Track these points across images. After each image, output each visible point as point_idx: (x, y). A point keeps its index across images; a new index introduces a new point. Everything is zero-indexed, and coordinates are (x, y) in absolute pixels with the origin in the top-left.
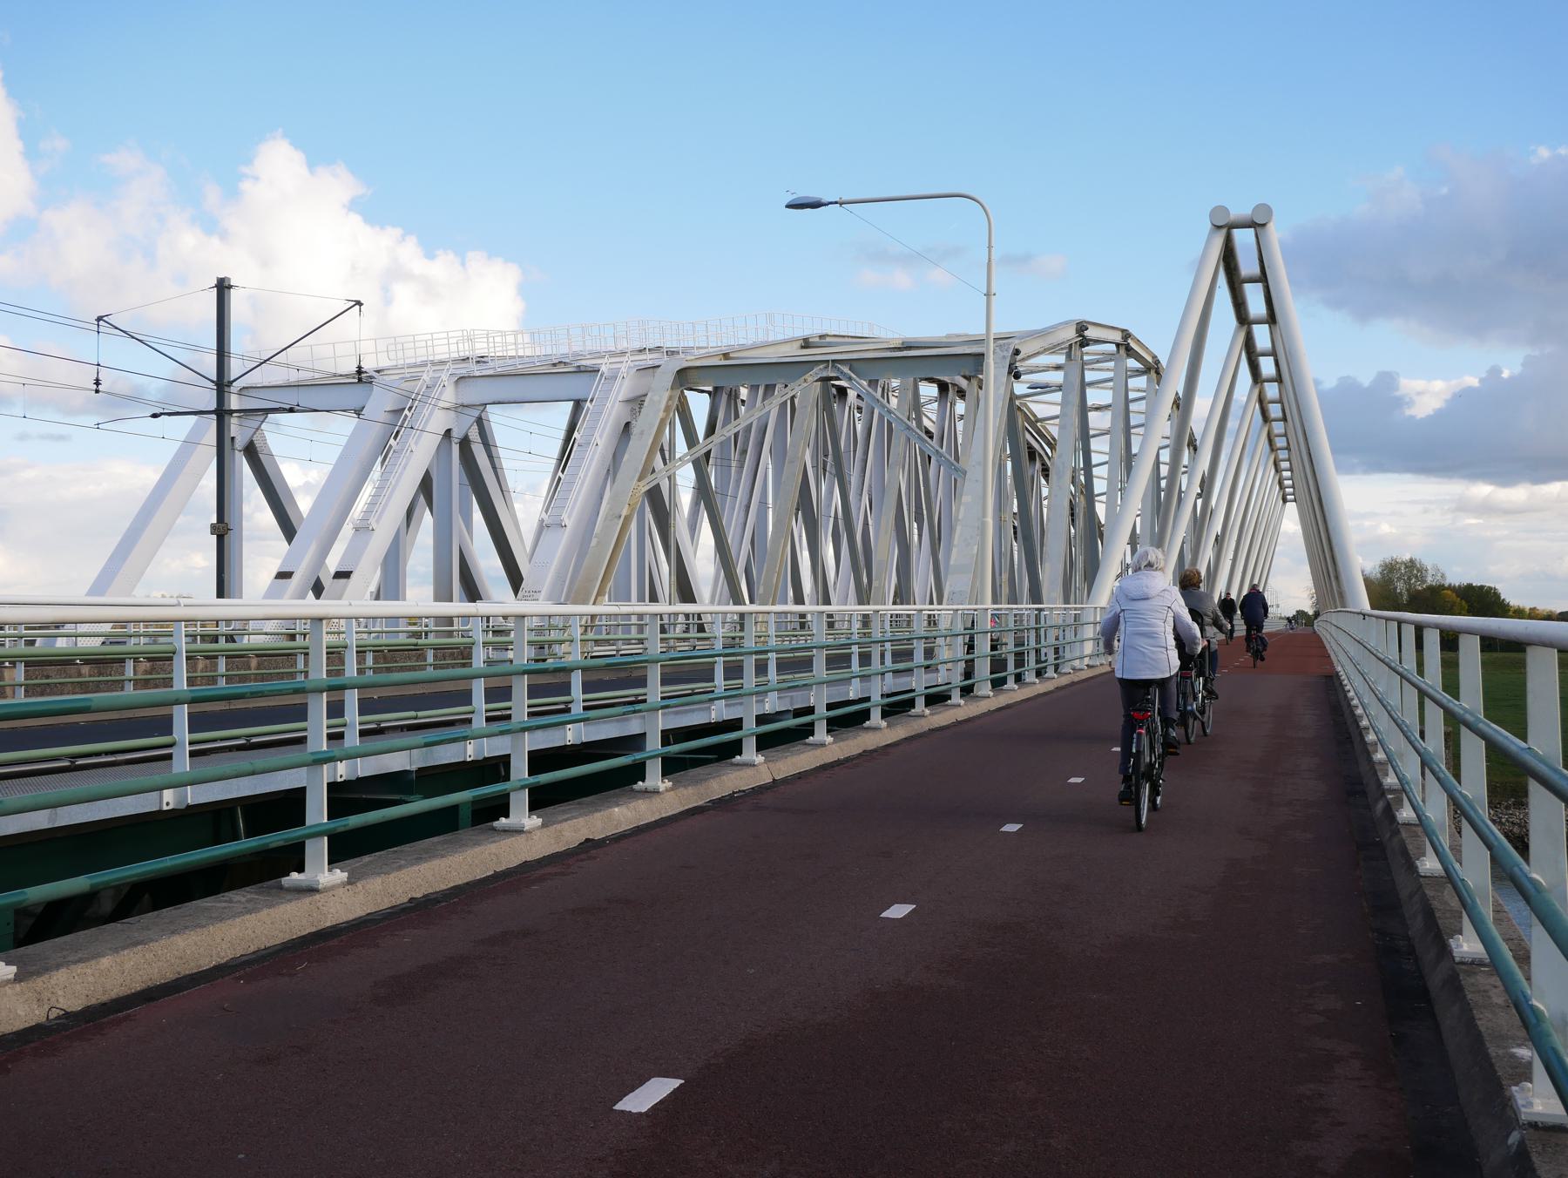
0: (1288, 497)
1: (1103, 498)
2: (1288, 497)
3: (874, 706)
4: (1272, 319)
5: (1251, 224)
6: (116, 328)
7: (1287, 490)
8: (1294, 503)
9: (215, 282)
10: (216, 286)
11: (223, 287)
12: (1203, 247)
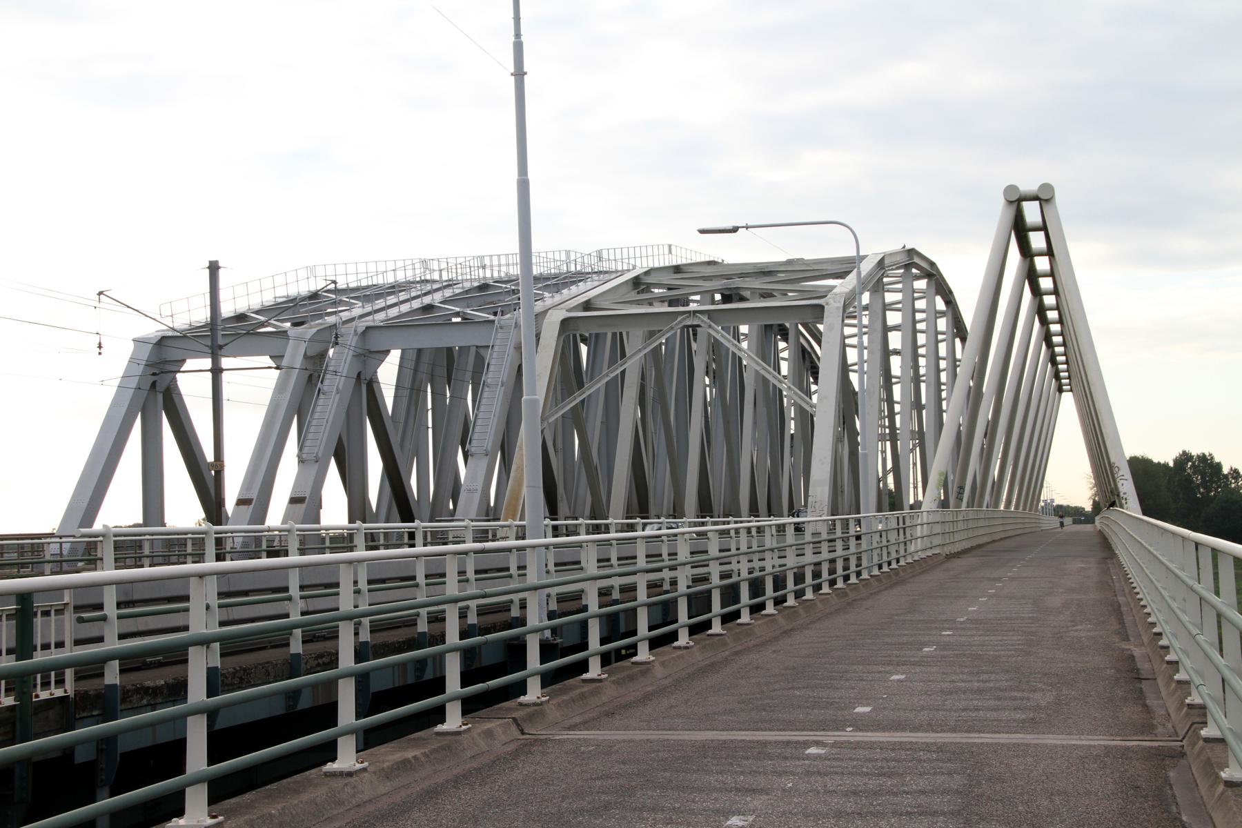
0: (1062, 374)
1: (856, 368)
2: (1062, 374)
3: (789, 592)
4: (1050, 252)
5: (1035, 198)
6: (129, 307)
7: (1063, 381)
8: (1071, 393)
9: (208, 265)
10: (208, 268)
11: (214, 268)
12: (996, 215)
